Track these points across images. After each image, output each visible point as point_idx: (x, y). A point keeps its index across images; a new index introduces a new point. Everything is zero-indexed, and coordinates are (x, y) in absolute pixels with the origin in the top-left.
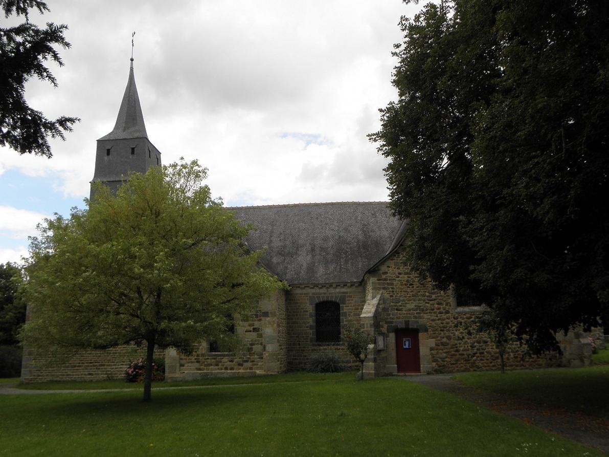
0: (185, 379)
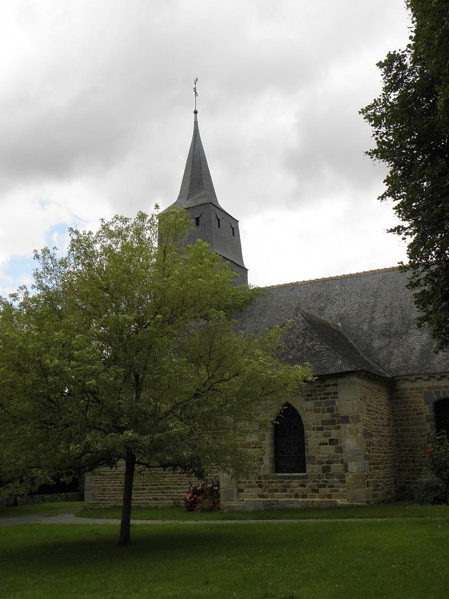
0: (244, 509)
